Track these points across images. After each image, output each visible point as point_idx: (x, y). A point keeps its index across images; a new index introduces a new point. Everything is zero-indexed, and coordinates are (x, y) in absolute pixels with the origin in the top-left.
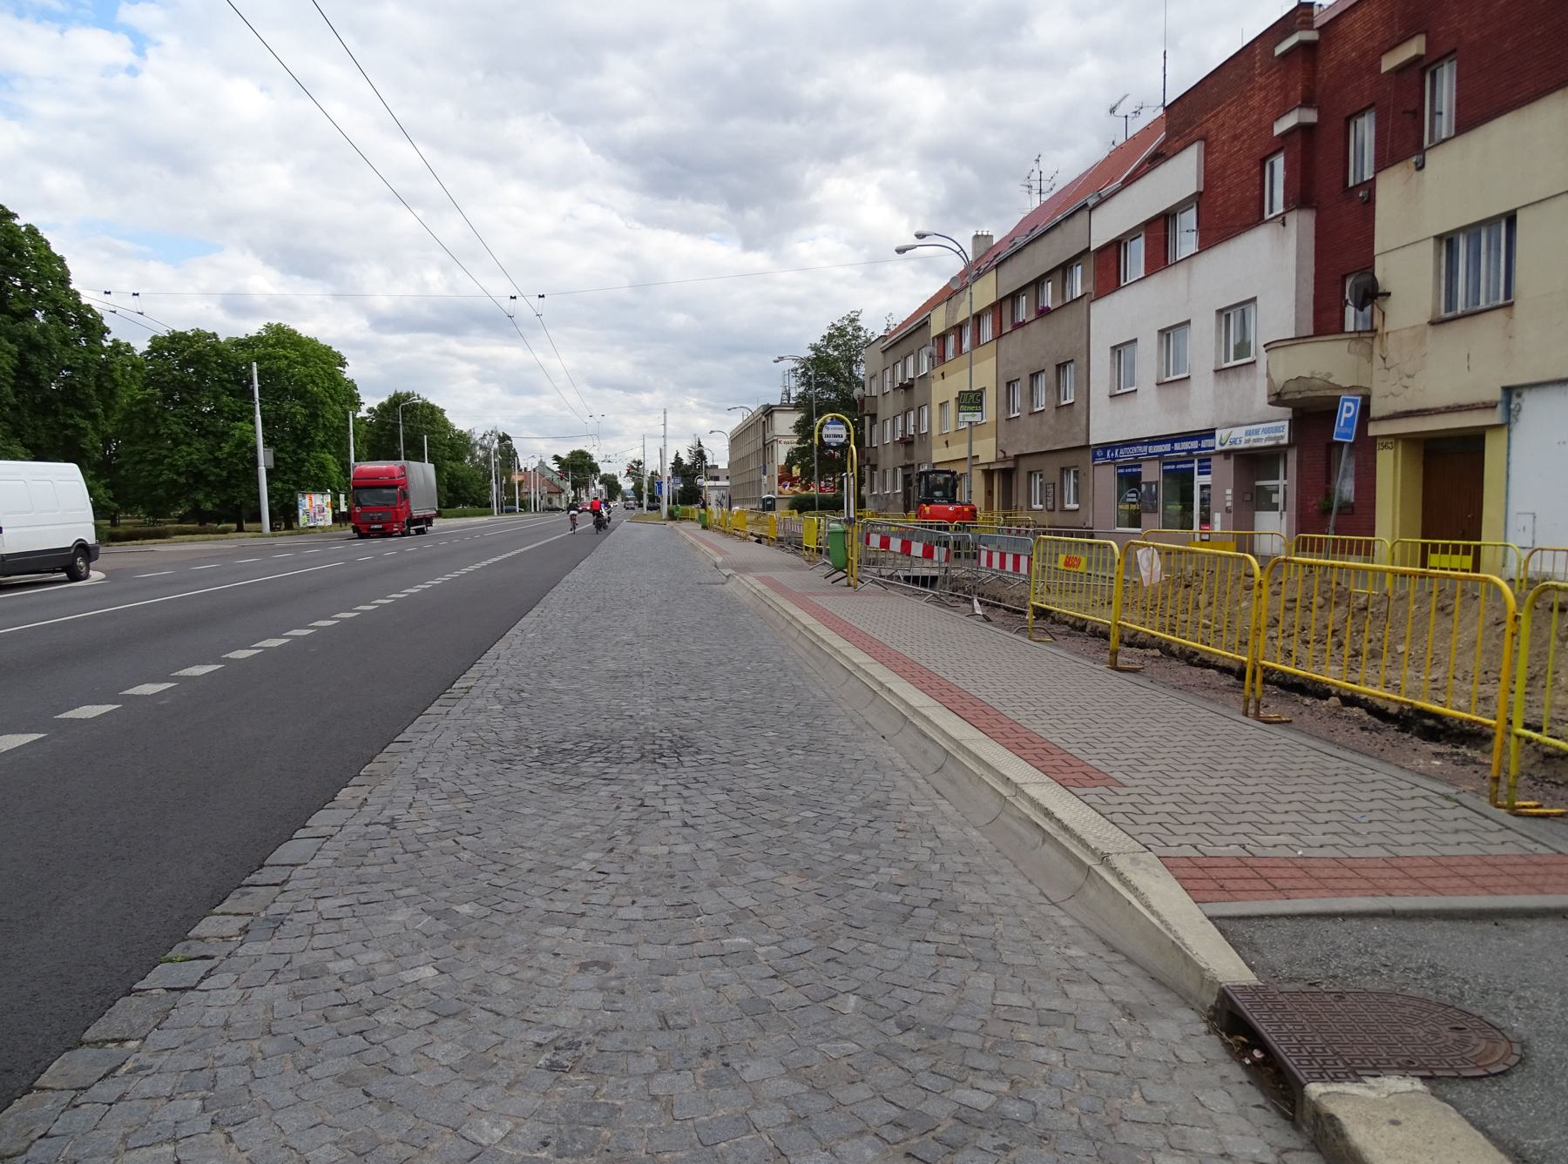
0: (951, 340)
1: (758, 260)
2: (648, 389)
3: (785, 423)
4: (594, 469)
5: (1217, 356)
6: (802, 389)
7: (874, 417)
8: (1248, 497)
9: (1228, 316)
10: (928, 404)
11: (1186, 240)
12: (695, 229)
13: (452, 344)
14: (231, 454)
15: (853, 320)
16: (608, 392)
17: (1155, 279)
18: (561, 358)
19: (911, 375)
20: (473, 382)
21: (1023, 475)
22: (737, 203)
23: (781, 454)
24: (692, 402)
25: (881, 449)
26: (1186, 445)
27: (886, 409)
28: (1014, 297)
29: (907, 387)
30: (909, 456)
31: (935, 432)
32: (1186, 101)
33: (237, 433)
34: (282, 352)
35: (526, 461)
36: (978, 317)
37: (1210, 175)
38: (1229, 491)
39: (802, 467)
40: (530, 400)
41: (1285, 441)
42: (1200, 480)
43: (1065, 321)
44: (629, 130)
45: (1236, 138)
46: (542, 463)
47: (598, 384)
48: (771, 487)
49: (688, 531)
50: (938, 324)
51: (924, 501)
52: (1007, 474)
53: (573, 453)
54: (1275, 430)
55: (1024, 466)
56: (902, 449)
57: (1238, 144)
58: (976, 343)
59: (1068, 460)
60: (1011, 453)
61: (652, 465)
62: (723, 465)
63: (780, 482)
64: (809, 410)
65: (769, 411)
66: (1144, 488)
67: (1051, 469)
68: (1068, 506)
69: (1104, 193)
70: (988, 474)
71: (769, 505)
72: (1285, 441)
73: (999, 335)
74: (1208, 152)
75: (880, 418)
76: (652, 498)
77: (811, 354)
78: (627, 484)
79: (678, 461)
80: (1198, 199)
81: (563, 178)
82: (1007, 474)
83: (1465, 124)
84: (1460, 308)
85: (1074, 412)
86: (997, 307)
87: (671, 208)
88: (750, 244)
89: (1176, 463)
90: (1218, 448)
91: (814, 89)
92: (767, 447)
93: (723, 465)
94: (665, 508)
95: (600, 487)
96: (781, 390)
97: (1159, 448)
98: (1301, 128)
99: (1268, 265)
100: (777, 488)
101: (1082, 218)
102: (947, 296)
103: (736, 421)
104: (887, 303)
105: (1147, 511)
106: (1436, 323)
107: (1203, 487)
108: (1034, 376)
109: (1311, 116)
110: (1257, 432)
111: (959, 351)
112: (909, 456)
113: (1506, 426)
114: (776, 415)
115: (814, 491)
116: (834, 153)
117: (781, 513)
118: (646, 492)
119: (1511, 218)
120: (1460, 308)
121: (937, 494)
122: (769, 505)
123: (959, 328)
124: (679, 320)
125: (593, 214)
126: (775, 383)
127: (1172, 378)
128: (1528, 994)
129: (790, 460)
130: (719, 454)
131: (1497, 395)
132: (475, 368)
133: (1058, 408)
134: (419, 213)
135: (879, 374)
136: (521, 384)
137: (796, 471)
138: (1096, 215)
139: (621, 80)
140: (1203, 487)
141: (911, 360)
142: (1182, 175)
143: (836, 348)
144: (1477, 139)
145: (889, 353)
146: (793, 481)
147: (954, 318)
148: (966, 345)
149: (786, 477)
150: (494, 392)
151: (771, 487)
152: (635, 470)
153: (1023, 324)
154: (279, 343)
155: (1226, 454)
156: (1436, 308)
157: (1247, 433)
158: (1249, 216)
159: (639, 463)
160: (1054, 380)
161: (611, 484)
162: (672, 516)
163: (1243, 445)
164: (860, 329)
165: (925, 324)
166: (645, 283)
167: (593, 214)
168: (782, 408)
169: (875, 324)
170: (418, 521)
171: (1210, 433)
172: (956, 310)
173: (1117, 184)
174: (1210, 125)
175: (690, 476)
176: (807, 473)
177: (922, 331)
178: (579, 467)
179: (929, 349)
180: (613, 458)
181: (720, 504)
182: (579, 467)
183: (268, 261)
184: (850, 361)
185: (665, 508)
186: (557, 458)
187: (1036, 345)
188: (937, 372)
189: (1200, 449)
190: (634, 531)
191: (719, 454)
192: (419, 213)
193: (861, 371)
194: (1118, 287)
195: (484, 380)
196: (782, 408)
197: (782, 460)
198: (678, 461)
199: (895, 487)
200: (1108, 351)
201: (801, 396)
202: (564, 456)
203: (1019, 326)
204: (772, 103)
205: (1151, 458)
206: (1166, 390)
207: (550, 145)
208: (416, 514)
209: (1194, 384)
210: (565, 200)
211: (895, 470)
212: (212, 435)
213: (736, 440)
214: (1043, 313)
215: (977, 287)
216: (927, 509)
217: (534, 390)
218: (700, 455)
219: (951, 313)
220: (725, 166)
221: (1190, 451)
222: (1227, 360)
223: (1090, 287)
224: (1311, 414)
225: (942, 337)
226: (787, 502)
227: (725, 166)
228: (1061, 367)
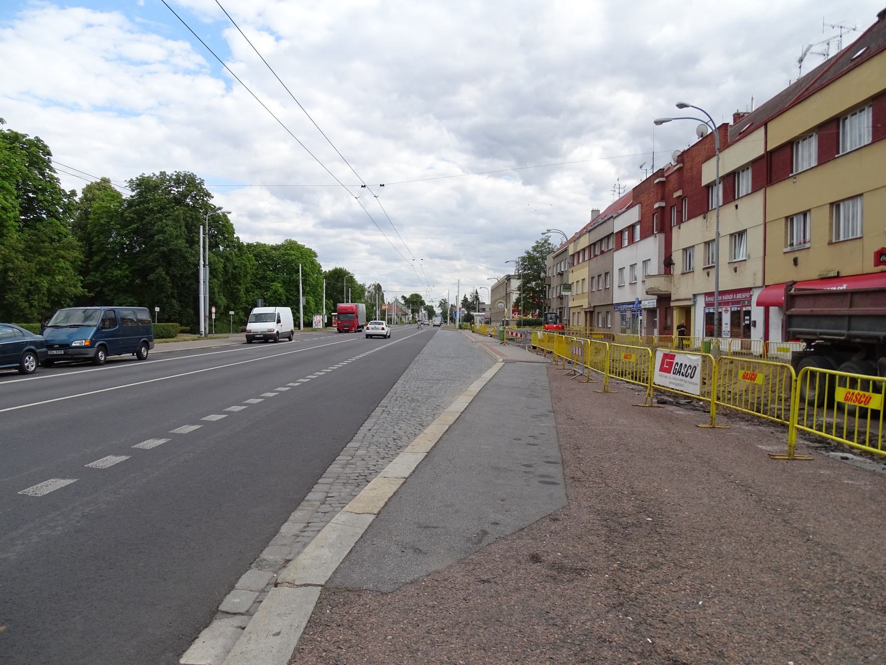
1: (530, 190)
2: (457, 258)
3: (515, 284)
4: (422, 303)
7: (550, 285)
11: (745, 183)
12: (496, 174)
13: (358, 234)
14: (271, 297)
16: (437, 261)
17: (830, 168)
18: (414, 242)
20: (364, 254)
21: (596, 313)
22: (522, 161)
23: (514, 297)
24: (482, 267)
28: (594, 244)
30: (561, 303)
33: (274, 287)
34: (293, 252)
35: (388, 298)
36: (584, 250)
37: (643, 215)
40: (397, 264)
43: (607, 256)
44: (467, 123)
46: (397, 300)
47: (433, 256)
49: (467, 333)
50: (571, 251)
52: (592, 313)
53: (412, 295)
54: (650, 302)
55: (597, 310)
59: (608, 308)
61: (452, 301)
63: (513, 312)
64: (526, 279)
65: (509, 278)
67: (603, 311)
69: (620, 211)
70: (586, 313)
76: (451, 319)
77: (526, 255)
78: (438, 311)
79: (465, 300)
80: (639, 222)
81: (428, 149)
82: (592, 313)
83: (689, 219)
84: (842, 239)
85: (608, 290)
87: (484, 164)
88: (527, 182)
91: (574, 100)
92: (508, 295)
94: (457, 323)
95: (424, 312)
98: (659, 207)
99: (650, 248)
101: (612, 220)
106: (683, 274)
108: (599, 276)
109: (663, 204)
113: (694, 305)
116: (577, 132)
118: (448, 315)
119: (805, 214)
120: (842, 239)
123: (579, 253)
124: (481, 222)
125: (442, 166)
128: (856, 579)
131: (691, 296)
132: (368, 247)
134: (353, 167)
136: (392, 255)
138: (616, 220)
139: (468, 97)
142: (633, 215)
143: (538, 252)
144: (692, 221)
148: (587, 258)
150: (377, 260)
152: (443, 304)
154: (292, 248)
155: (645, 309)
159: (445, 300)
161: (431, 313)
162: (460, 327)
165: (566, 250)
166: (466, 201)
167: (442, 166)
170: (359, 327)
173: (624, 209)
175: (471, 305)
178: (415, 302)
180: (431, 298)
181: (481, 322)
182: (415, 302)
183: (273, 193)
184: (544, 258)
185: (457, 323)
186: (403, 297)
187: (599, 264)
188: (570, 270)
190: (449, 335)
192: (353, 167)
194: (621, 247)
195: (372, 253)
198: (465, 300)
202: (408, 297)
203: (595, 256)
204: (549, 109)
207: (426, 131)
208: (360, 324)
210: (429, 159)
212: (158, 258)
213: (494, 290)
214: (602, 252)
215: (582, 239)
217: (397, 260)
218: (477, 298)
219: (575, 247)
220: (517, 142)
223: (614, 246)
224: (664, 299)
225: (573, 255)
227: (517, 142)
228: (606, 274)
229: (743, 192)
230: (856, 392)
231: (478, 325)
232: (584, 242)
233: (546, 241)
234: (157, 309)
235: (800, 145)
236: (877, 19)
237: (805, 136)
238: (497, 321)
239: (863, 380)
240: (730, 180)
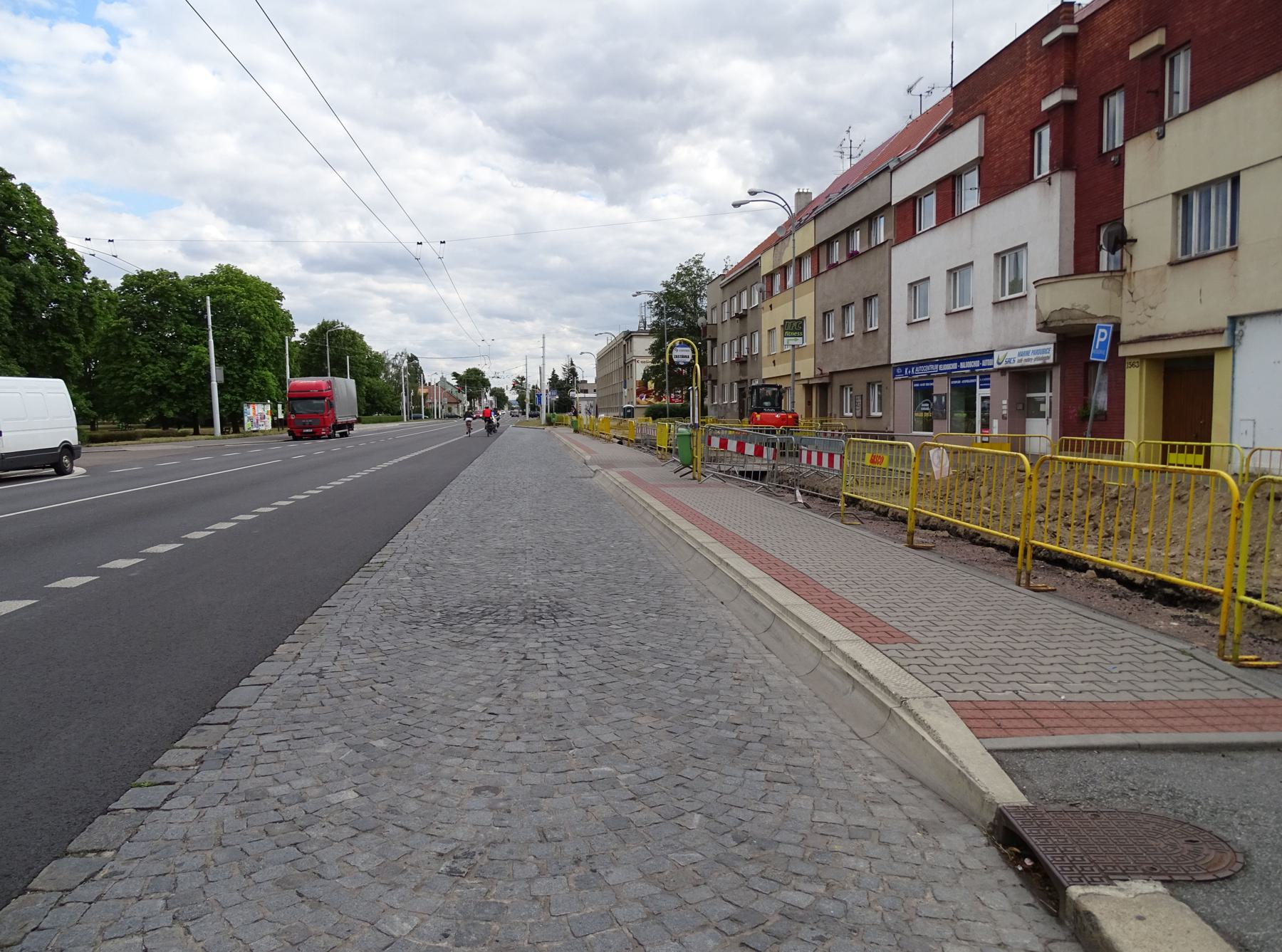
0: (778, 278)
1: (620, 212)
2: (530, 318)
3: (642, 346)
4: (486, 383)
5: (995, 291)
6: (655, 318)
7: (714, 341)
8: (1020, 407)
9: (1004, 259)
10: (759, 330)
11: (970, 196)
12: (568, 187)
13: (370, 281)
14: (189, 372)
15: (697, 262)
16: (497, 321)
17: (945, 229)
18: (459, 293)
19: (744, 306)
20: (386, 312)
21: (836, 388)
22: (603, 166)
23: (639, 371)
24: (565, 329)
25: (720, 367)
26: (970, 364)
27: (725, 334)
28: (829, 243)
29: (742, 317)
30: (743, 373)
31: (765, 353)
32: (970, 83)
33: (194, 354)
34: (230, 288)
35: (430, 377)
36: (799, 259)
37: (989, 143)
38: (1005, 402)
39: (656, 382)
40: (433, 327)
41: (1051, 361)
42: (981, 393)
43: (871, 263)
44: (514, 107)
45: (1010, 112)
46: (443, 379)
47: (489, 314)
48: (630, 398)
49: (562, 434)
50: (767, 265)
51: (755, 410)
52: (824, 388)
53: (469, 371)
54: (1042, 352)
55: (837, 381)
56: (737, 367)
57: (1012, 118)
58: (798, 280)
59: (873, 376)
60: (827, 370)
61: (533, 380)
62: (591, 380)
63: (638, 394)
64: (661, 335)
65: (629, 336)
66: (935, 399)
67: (859, 384)
68: (873, 414)
69: (903, 157)
70: (808, 388)
71: (629, 413)
72: (1051, 361)
73: (817, 274)
74: (987, 124)
75: (719, 342)
76: (533, 408)
77: (663, 289)
78: (512, 396)
79: (554, 377)
80: (979, 163)
81: (461, 145)
82: (824, 388)
83: (1198, 102)
84: (1194, 252)
85: (878, 337)
86: (815, 251)
87: (549, 170)
88: (613, 199)
89: (961, 379)
90: (996, 366)
91: (665, 73)
92: (627, 366)
93: (591, 380)
94: (543, 415)
95: (490, 398)
96: (639, 319)
97: (948, 367)
98: (1064, 105)
99: (1037, 217)
100: (635, 399)
101: (884, 178)
102: (774, 242)
103: (601, 344)
104: (725, 248)
105: (937, 418)
106: (1174, 264)
107: (983, 399)
108: (845, 308)
109: (1072, 95)
110: (1028, 353)
111: (784, 287)
112: (743, 373)
113: (1231, 348)
114: (635, 339)
115: (665, 401)
116: (682, 125)
117: (638, 419)
118: (528, 403)
119: (1235, 179)
120: (1194, 252)
121: (766, 404)
122: (629, 413)
123: (784, 269)
124: (555, 261)
125: (485, 175)
126: (633, 313)
127: (958, 309)
128: (1250, 813)
129: (646, 377)
130: (588, 372)
131: (1224, 323)
132: (388, 301)
133: (865, 333)
134: (343, 174)
135: (719, 306)
136: (426, 314)
137: (651, 385)
138: (896, 176)
139: (508, 66)
140: (983, 399)
141: (745, 295)
142: (966, 143)
143: (684, 284)
144: (1207, 114)
145: (727, 289)
146: (648, 394)
147: (780, 260)
148: (790, 282)
149: (642, 390)
150: (404, 321)
151: (630, 398)
152: (519, 384)
153: (836, 265)
154: (228, 280)
155: (1003, 371)
156: (1174, 252)
157: (1020, 354)
158: (1021, 177)
159: (523, 379)
160: (861, 311)
161: (500, 396)
162: (549, 422)
163: (1016, 364)
164: (703, 269)
165: (756, 265)
166: (527, 231)
167: (485, 175)
168: (639, 334)
169: (715, 265)
170: (342, 426)
171: (989, 354)
172: (781, 254)
173: (913, 150)
174: (989, 102)
175: (564, 389)
176: (660, 387)
177: (754, 271)
178: (473, 382)
179: (759, 285)
180: (501, 374)
181: (589, 412)
182: (473, 382)
183: (219, 213)
184: (695, 296)
185: (543, 415)
186: (455, 374)
187: (847, 282)
188: (766, 304)
189: (981, 367)
190: (518, 435)
191: (588, 372)
192: (343, 174)
193: (704, 304)
194: (914, 235)
195: (396, 311)
196: (639, 334)
197: (639, 377)
198: (554, 377)
199: (731, 398)
200: (906, 287)
201: (655, 324)
202: (461, 373)
203: (833, 266)
204: (631, 85)
205: (941, 374)
206: (953, 319)
207: (450, 119)
208: (340, 420)
209: (976, 314)
210: (462, 164)
211: (732, 384)
212: (173, 356)
213: (602, 360)
214: (853, 256)
215: (799, 235)
216: (758, 416)
217: (437, 319)
218: (573, 372)
219: (777, 256)
220: (593, 135)
221: (973, 369)
222: (1003, 295)
223: (891, 234)
224: (1072, 339)
225: (771, 276)
226: (644, 411)
227: (593, 135)
228: (867, 300)
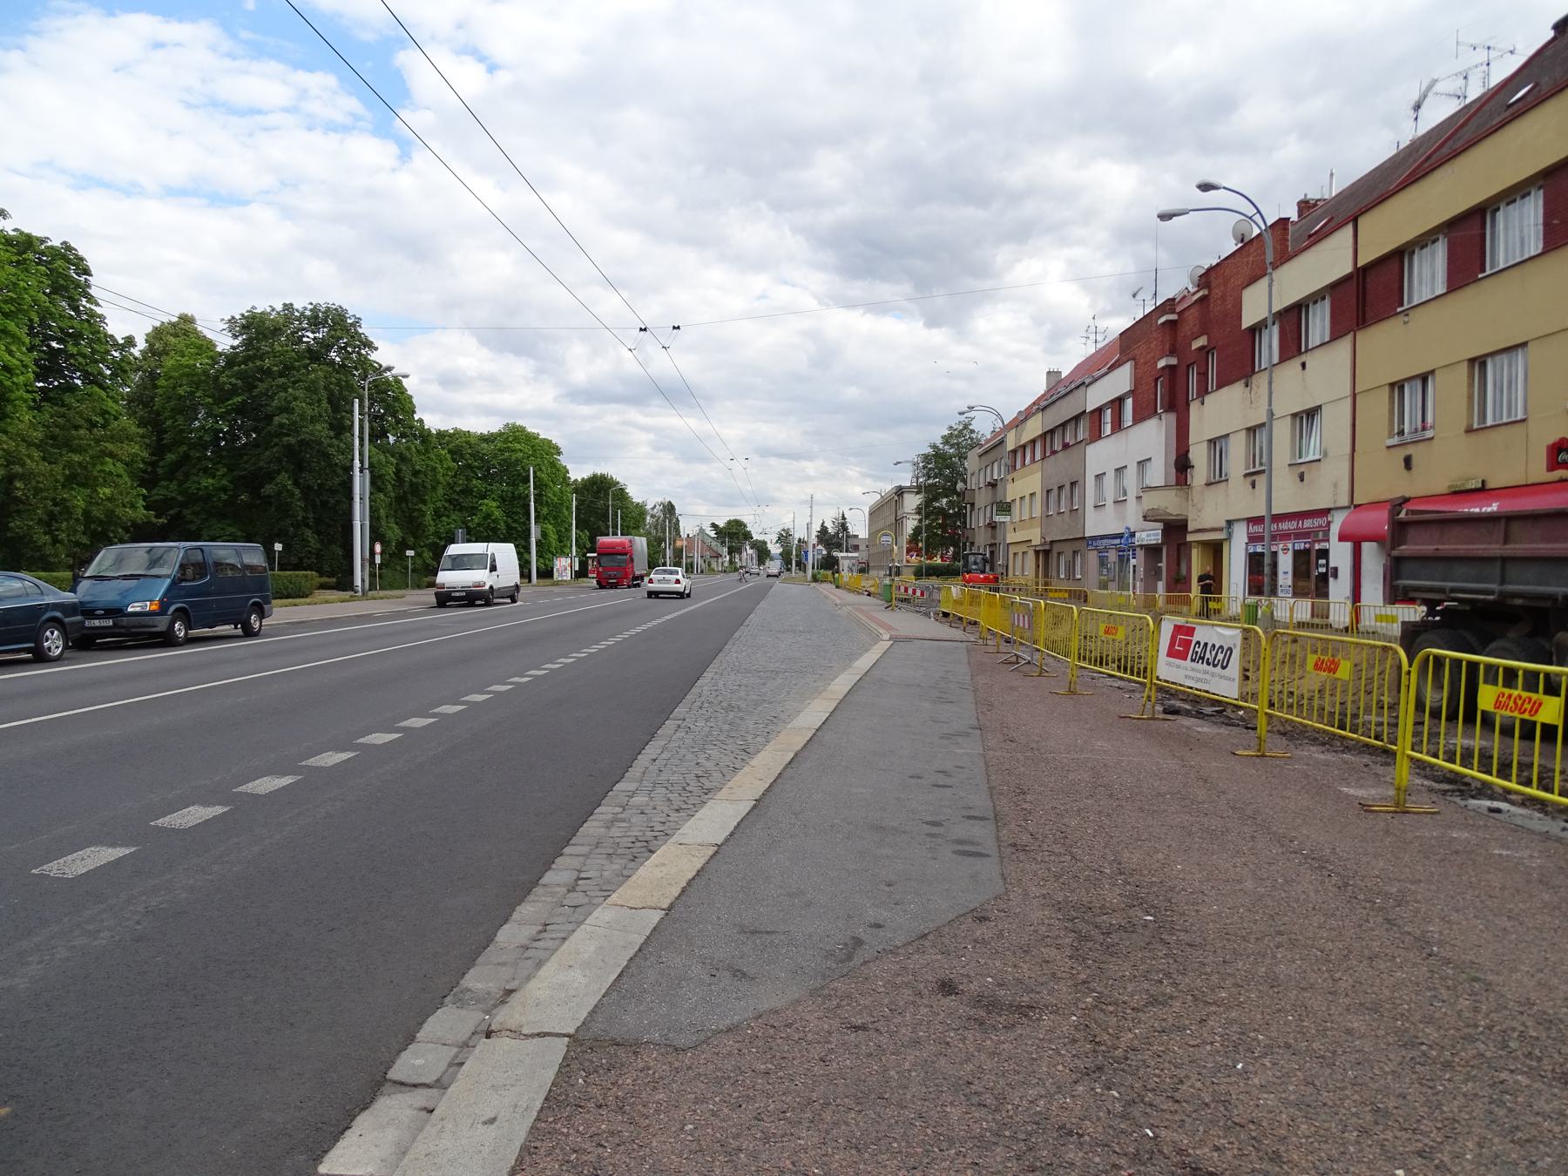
1: (938, 336)
2: (809, 457)
3: (912, 502)
4: (748, 536)
7: (973, 505)
11: (1318, 324)
12: (878, 308)
13: (634, 414)
14: (479, 525)
16: (773, 461)
17: (1468, 297)
18: (732, 429)
20: (644, 449)
21: (1055, 554)
22: (923, 285)
23: (910, 525)
24: (852, 472)
28: (1052, 432)
30: (994, 537)
33: (484, 508)
34: (518, 446)
35: (687, 528)
36: (1033, 441)
37: (1137, 381)
40: (703, 468)
43: (1074, 453)
44: (827, 218)
46: (702, 531)
47: (767, 452)
49: (826, 589)
50: (1010, 445)
52: (1047, 553)
53: (729, 522)
54: (1151, 535)
55: (1056, 548)
59: (1077, 545)
61: (800, 533)
63: (908, 551)
64: (930, 493)
65: (900, 492)
67: (1068, 549)
69: (1097, 374)
70: (1037, 553)
76: (799, 564)
77: (930, 450)
78: (775, 549)
79: (824, 530)
80: (1132, 393)
81: (758, 263)
82: (1047, 553)
83: (1219, 387)
84: (1489, 422)
85: (1076, 513)
87: (857, 289)
88: (932, 322)
91: (1015, 177)
92: (898, 522)
94: (810, 572)
95: (750, 552)
98: (1167, 367)
99: (1150, 439)
101: (1082, 389)
106: (1208, 484)
108: (1060, 488)
109: (1173, 361)
113: (1229, 539)
116: (1022, 234)
118: (793, 556)
119: (1424, 378)
120: (1489, 422)
123: (1024, 447)
124: (852, 393)
125: (783, 294)
128: (1514, 1024)
131: (1223, 524)
132: (651, 436)
134: (625, 295)
136: (693, 452)
138: (1090, 390)
139: (828, 171)
142: (1120, 381)
143: (952, 446)
144: (1225, 390)
148: (1038, 457)
150: (667, 460)
152: (784, 538)
154: (516, 439)
155: (1141, 546)
159: (787, 531)
161: (762, 553)
162: (815, 579)
165: (1002, 442)
166: (825, 355)
167: (783, 294)
170: (635, 578)
173: (1104, 370)
175: (834, 539)
178: (734, 534)
180: (763, 528)
181: (851, 570)
182: (734, 534)
183: (484, 342)
184: (963, 457)
185: (810, 572)
186: (714, 526)
187: (1060, 466)
188: (1010, 477)
190: (794, 592)
192: (625, 295)
194: (1100, 437)
195: (657, 448)
198: (824, 530)
202: (721, 525)
203: (1054, 452)
204: (972, 193)
207: (754, 231)
208: (637, 573)
210: (760, 282)
212: (279, 456)
213: (875, 513)
214: (1066, 446)
215: (1030, 422)
217: (703, 460)
218: (844, 527)
219: (1018, 436)
220: (915, 251)
223: (1087, 435)
224: (1175, 529)
225: (1014, 452)
227: (915, 251)
228: (1073, 484)
229: (1315, 339)
230: (1515, 693)
231: (845, 575)
232: (1034, 428)
233: (966, 427)
234: (278, 547)
235: (1416, 257)
236: (1552, 34)
237: (1425, 240)
238: (880, 568)
239: (1527, 672)
240: (1292, 318)
